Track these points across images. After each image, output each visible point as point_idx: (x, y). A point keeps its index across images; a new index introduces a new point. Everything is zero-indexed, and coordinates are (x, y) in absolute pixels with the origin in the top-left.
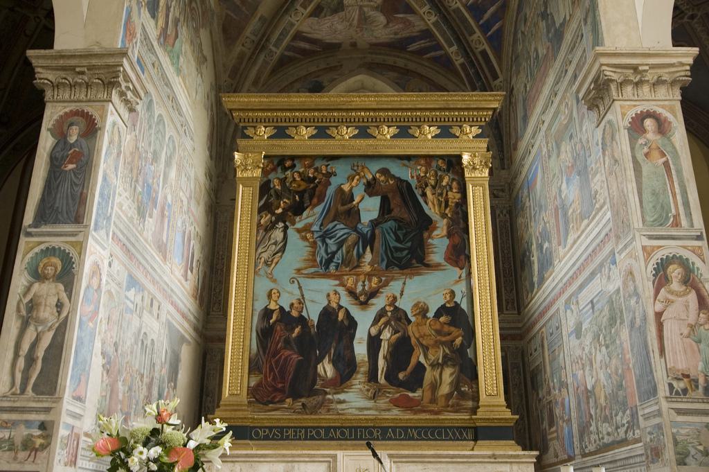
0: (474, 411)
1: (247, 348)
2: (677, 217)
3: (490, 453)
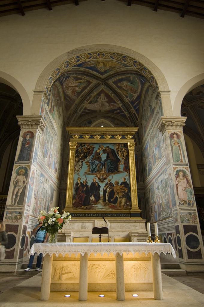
0: (130, 209)
1: (72, 193)
2: (182, 160)
3: (134, 220)
